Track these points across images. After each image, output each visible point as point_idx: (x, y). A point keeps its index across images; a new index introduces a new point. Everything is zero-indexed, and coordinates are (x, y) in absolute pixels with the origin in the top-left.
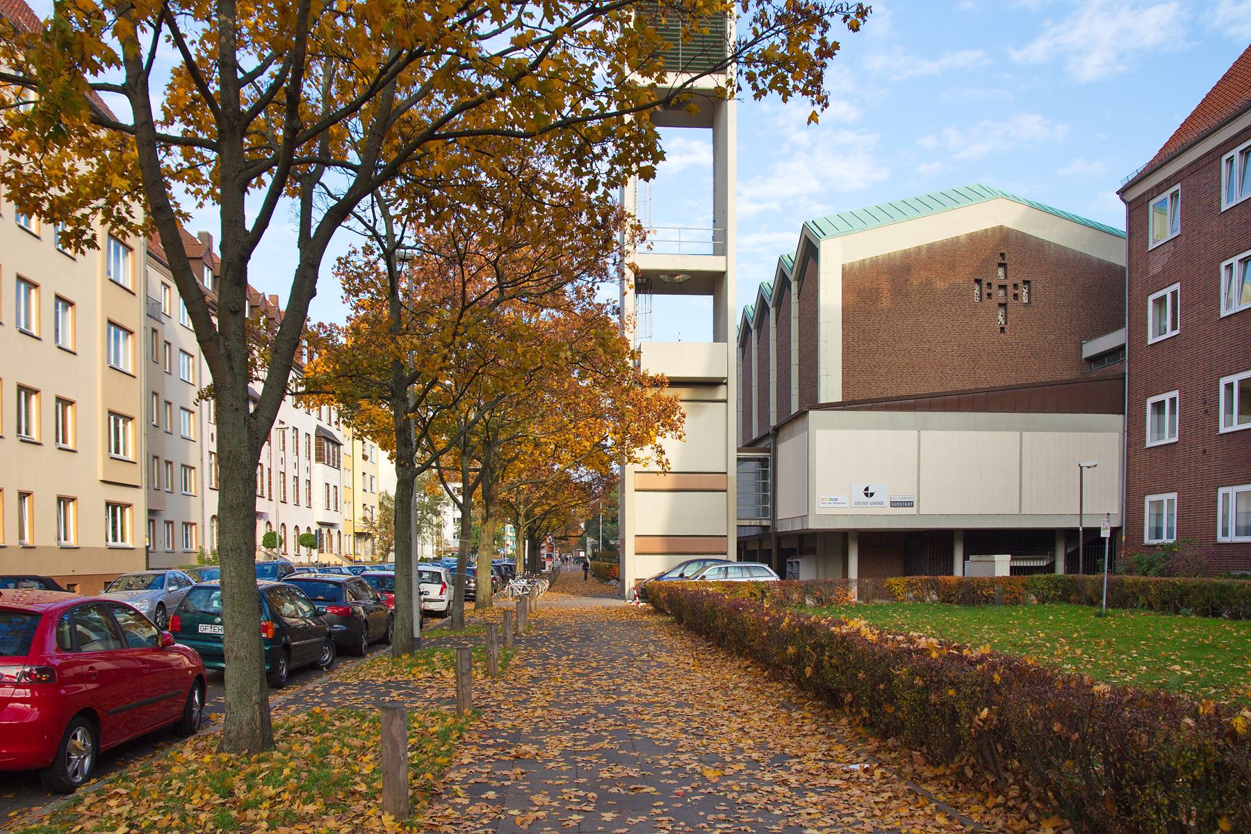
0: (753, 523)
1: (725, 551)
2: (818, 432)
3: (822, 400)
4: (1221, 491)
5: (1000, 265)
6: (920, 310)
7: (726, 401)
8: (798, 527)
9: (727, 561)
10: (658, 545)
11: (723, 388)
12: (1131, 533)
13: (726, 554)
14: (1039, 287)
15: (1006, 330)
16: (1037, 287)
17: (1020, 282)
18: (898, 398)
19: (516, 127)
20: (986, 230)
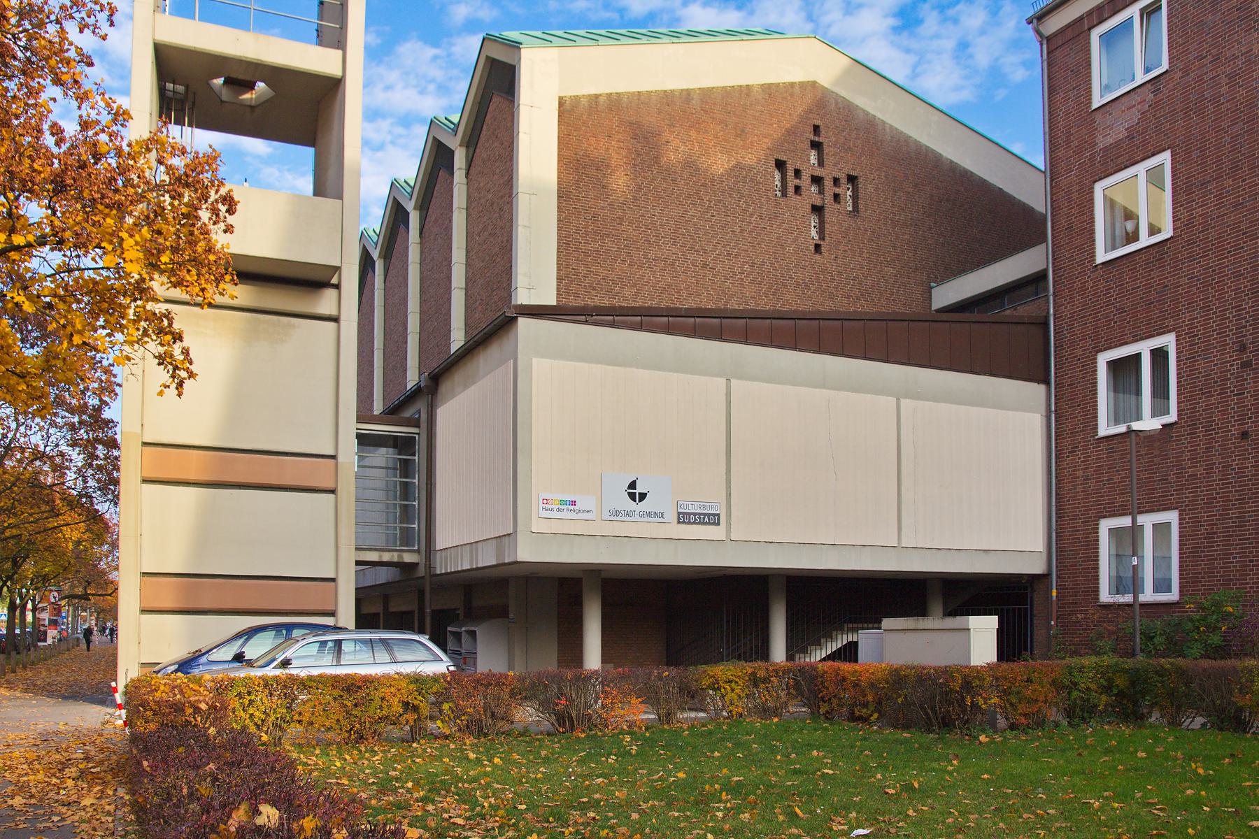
0: (386, 557)
1: (329, 608)
6: (689, 196)
7: (335, 319)
8: (487, 559)
9: (336, 629)
11: (330, 294)
12: (1069, 585)
13: (332, 614)
14: (870, 189)
15: (823, 249)
16: (866, 188)
18: (689, 313)
19: (98, 323)
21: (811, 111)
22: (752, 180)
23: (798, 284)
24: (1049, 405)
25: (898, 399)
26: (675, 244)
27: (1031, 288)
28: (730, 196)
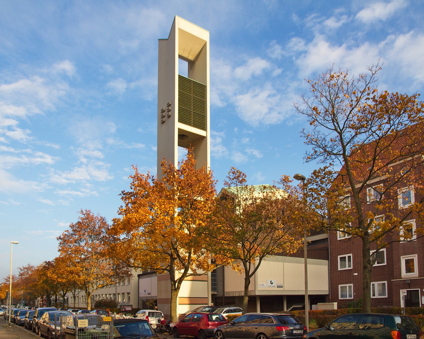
1: (207, 303)
4: (372, 283)
10: (187, 301)
24: (329, 264)
27: (323, 240)
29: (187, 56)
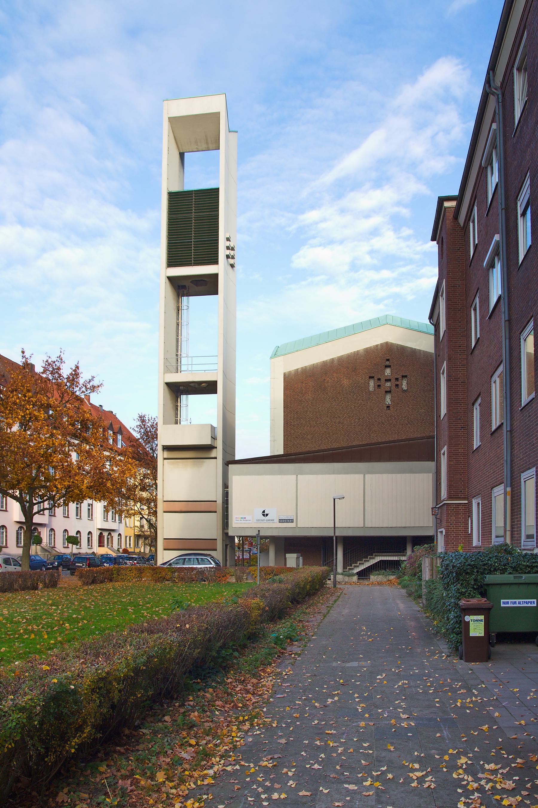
1: (215, 548)
2: (234, 477)
3: (237, 458)
5: (387, 367)
11: (215, 450)
17: (399, 377)
20: (377, 346)
21: (386, 354)
22: (359, 387)
23: (379, 423)
25: (364, 475)
26: (327, 417)
28: (350, 395)
29: (206, 147)
